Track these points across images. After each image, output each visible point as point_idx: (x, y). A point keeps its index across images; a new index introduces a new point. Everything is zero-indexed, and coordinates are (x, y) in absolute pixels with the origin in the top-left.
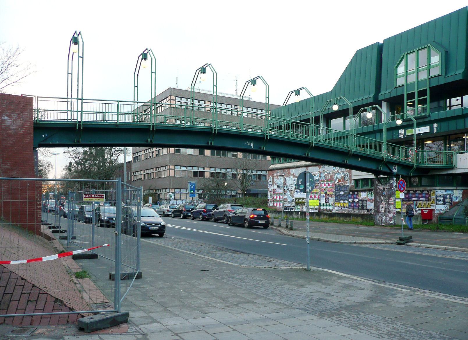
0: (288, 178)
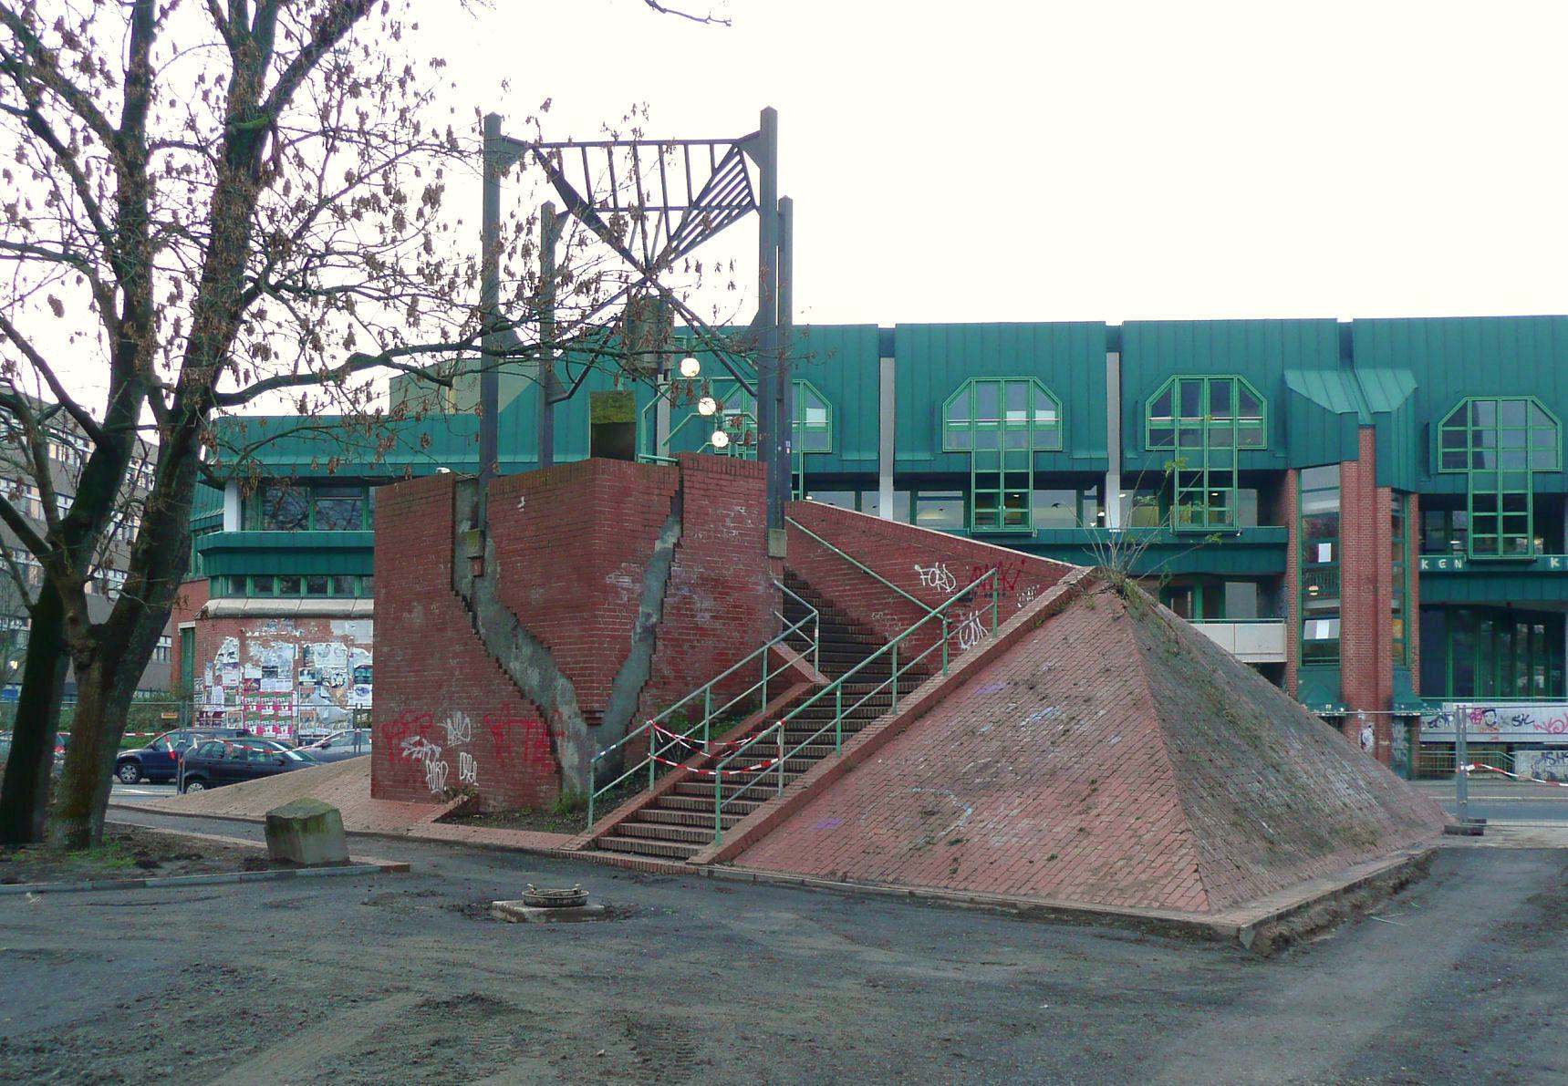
0: (317, 648)
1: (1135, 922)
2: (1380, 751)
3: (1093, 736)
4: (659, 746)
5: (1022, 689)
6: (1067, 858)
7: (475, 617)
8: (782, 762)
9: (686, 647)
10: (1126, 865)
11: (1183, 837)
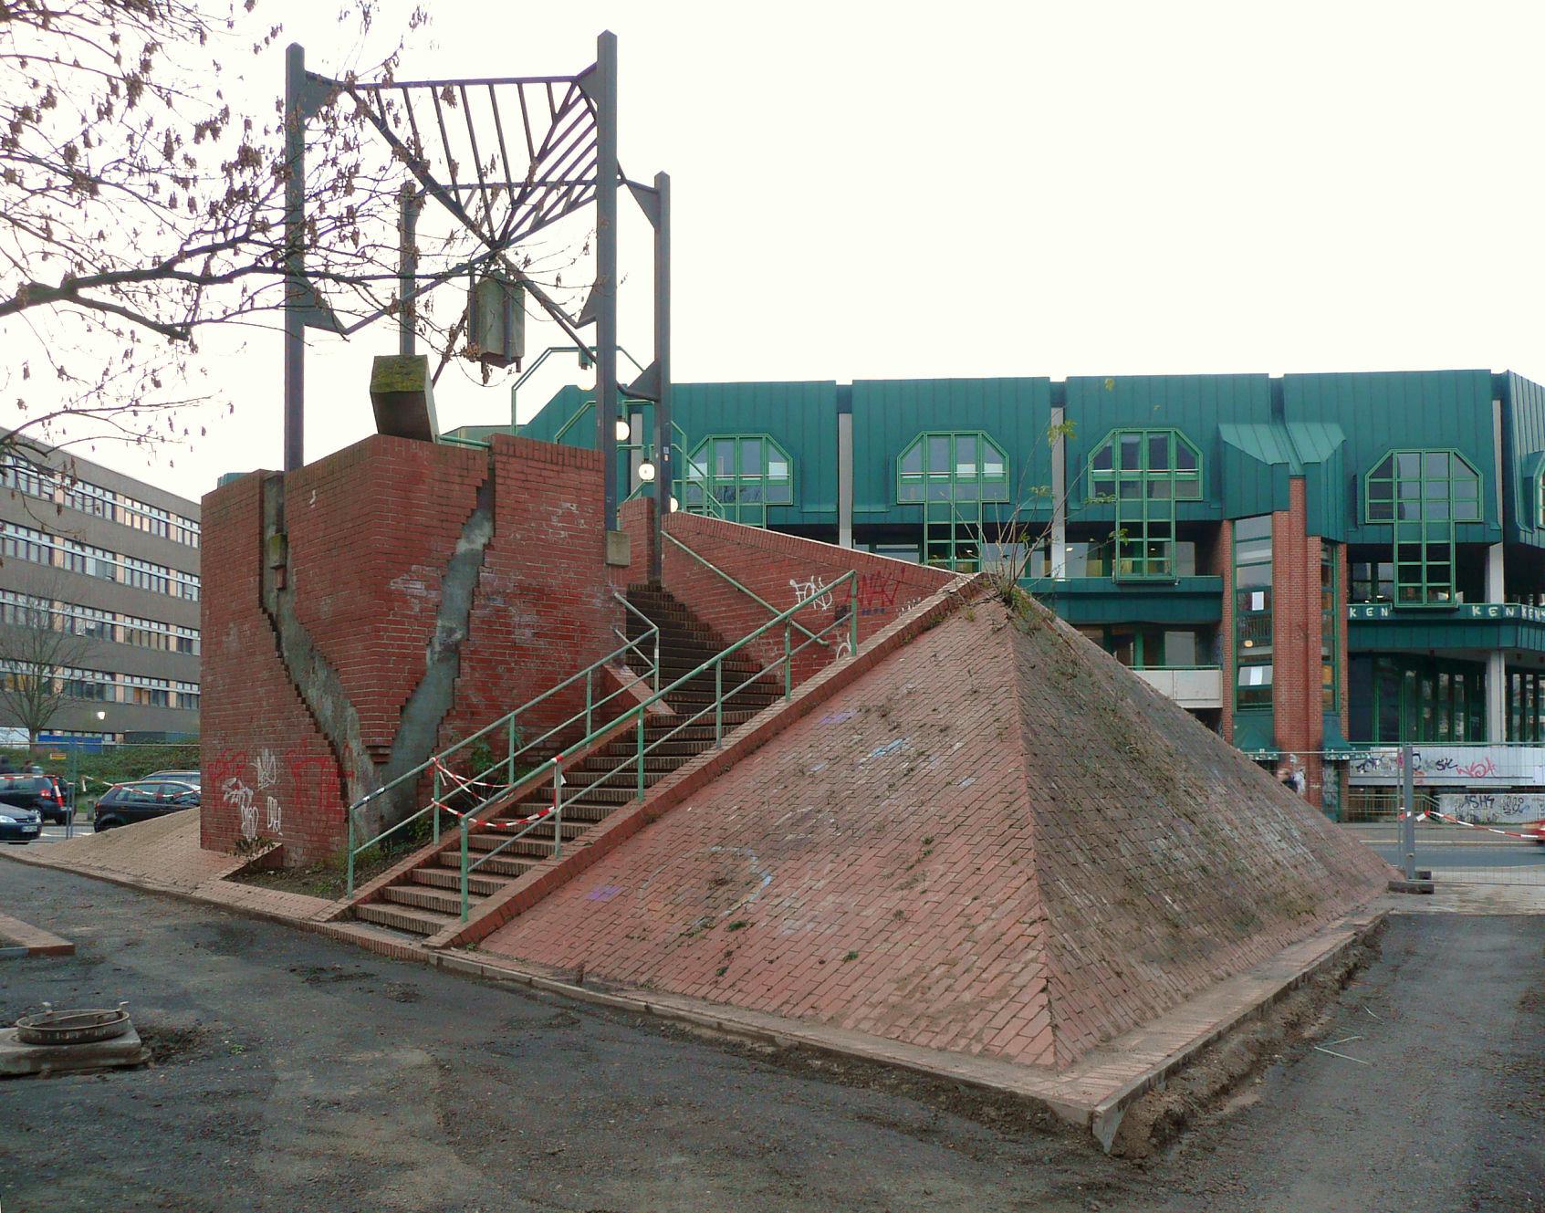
1: (932, 1086)
2: (1312, 794)
3: (940, 777)
4: (443, 791)
5: (874, 716)
6: (872, 959)
7: (279, 638)
8: (559, 810)
9: (501, 669)
10: (947, 975)
11: (1032, 931)
